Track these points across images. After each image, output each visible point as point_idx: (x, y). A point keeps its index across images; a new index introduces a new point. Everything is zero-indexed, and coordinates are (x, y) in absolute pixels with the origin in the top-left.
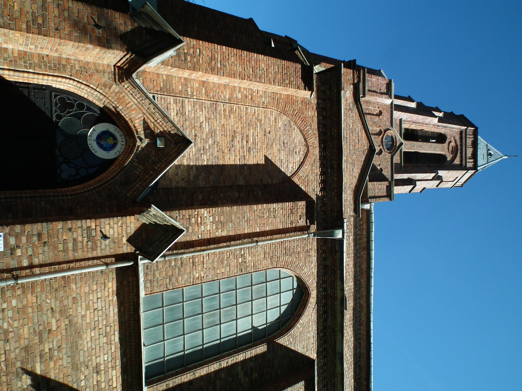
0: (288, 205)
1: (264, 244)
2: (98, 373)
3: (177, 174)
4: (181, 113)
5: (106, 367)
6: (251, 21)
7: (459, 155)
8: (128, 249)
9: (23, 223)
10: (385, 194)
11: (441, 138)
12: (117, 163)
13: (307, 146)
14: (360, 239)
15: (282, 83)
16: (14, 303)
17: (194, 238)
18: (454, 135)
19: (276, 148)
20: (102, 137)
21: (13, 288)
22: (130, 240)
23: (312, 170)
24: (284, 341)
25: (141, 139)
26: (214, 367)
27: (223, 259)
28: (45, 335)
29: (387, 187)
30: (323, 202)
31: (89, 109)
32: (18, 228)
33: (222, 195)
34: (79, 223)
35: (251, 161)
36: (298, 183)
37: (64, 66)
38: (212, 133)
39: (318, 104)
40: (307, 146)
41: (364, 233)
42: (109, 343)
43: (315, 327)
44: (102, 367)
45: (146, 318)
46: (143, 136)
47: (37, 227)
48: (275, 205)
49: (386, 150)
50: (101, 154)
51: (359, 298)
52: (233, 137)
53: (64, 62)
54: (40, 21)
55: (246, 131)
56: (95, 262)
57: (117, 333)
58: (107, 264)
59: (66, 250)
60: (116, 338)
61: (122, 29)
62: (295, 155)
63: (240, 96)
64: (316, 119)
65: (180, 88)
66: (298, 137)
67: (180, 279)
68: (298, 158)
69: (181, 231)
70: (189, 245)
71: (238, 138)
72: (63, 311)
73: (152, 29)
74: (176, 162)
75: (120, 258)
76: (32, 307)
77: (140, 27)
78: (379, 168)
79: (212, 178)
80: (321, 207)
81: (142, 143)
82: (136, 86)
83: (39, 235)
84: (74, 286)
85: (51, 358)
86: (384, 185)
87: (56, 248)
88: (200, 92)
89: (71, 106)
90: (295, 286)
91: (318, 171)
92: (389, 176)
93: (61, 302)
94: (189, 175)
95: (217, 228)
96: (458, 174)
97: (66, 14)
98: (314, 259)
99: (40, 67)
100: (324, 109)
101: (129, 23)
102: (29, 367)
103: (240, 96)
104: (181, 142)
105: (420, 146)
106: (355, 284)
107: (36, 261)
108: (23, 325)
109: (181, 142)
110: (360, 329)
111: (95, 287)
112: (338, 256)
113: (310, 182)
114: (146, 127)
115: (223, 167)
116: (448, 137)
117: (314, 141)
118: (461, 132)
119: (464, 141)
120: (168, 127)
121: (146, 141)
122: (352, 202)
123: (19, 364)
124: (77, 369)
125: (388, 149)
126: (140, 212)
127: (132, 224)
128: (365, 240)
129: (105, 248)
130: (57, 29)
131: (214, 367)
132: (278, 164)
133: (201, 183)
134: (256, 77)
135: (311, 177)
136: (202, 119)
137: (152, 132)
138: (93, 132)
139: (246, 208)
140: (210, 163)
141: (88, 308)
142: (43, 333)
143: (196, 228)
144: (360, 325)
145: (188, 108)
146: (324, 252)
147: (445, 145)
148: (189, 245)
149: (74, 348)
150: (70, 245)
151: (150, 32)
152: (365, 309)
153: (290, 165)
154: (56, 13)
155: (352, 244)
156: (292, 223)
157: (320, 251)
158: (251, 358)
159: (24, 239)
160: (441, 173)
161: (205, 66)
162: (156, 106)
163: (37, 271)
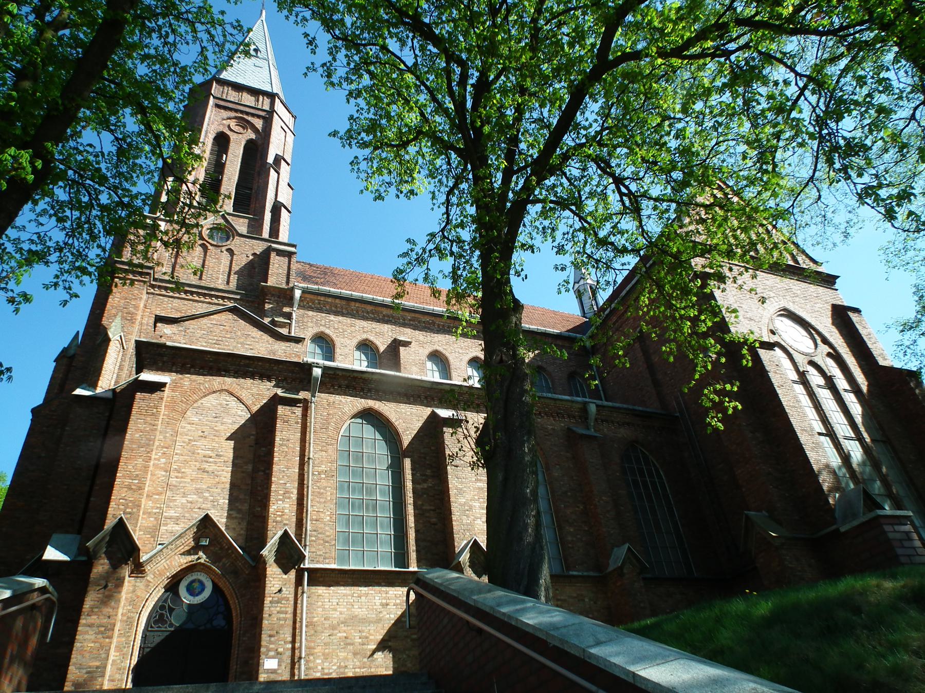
0: (279, 425)
1: (313, 451)
2: (387, 605)
3: (234, 529)
4: (177, 520)
5: (385, 598)
6: (34, 411)
7: (250, 118)
8: (292, 574)
9: (259, 646)
10: (286, 259)
11: (222, 141)
12: (216, 581)
13: (221, 391)
14: (336, 307)
15: (155, 416)
16: (319, 661)
17: (294, 519)
18: (219, 119)
19: (220, 427)
20: (191, 591)
21: (307, 662)
22: (286, 572)
23: (248, 389)
24: (406, 440)
25: (199, 558)
26: (410, 510)
27: (319, 493)
28: (349, 641)
29: (277, 255)
30: (282, 381)
31: (165, 601)
32: (263, 650)
33: (259, 488)
34: (266, 609)
35: (230, 455)
36: (259, 406)
37: (128, 618)
38: (198, 492)
39: (177, 372)
40: (221, 391)
41: (330, 300)
42: (367, 595)
43: (403, 406)
44: (384, 601)
45: (355, 565)
46: (196, 557)
47: (264, 637)
48: (277, 439)
49: (228, 242)
50: (207, 593)
51: (404, 320)
52: (204, 471)
53: (125, 618)
54: (103, 629)
55: (199, 457)
56: (299, 602)
57: (360, 588)
58: (303, 593)
59: (285, 619)
60: (364, 589)
61: (107, 567)
62: (227, 405)
63: (163, 460)
64: (194, 377)
65: (152, 519)
66: (211, 400)
67: (328, 533)
68: (233, 402)
69: (286, 532)
70: (300, 524)
71: (206, 466)
72: (333, 627)
73: (108, 542)
74: (223, 529)
75: (299, 582)
77: (105, 553)
78: (251, 257)
79: (242, 496)
80: (287, 383)
81: (203, 557)
82: (150, 560)
83: (271, 636)
84: (315, 619)
85: (367, 638)
86: (275, 259)
87: (282, 626)
88: (158, 500)
89: (161, 615)
90: (360, 421)
91: (249, 381)
92: (265, 245)
93: (325, 629)
94: (236, 518)
95: (289, 498)
96: (276, 123)
97: (96, 610)
98: (338, 398)
99: (129, 636)
100: (183, 365)
101: (102, 561)
102: (369, 653)
103: (163, 460)
104: (206, 523)
105: (230, 179)
106: (387, 322)
107: (290, 639)
108: (337, 656)
109: (206, 523)
110: (439, 325)
111: (320, 603)
112: (340, 373)
113: (259, 392)
114: (188, 553)
115: (233, 485)
116: (221, 129)
117: (217, 382)
118: (217, 106)
119: (231, 105)
120: (190, 535)
121: (201, 553)
122: (288, 344)
123: (365, 660)
124: (380, 620)
125: (228, 239)
126: (265, 563)
127: (273, 571)
128: (337, 301)
129: (289, 592)
130: (109, 617)
131: (410, 510)
132: (237, 426)
133: (245, 507)
134: (148, 445)
135: (255, 391)
136: (184, 500)
137: (193, 548)
138: (186, 599)
139: (275, 468)
140: (227, 497)
141: (335, 610)
142: (347, 642)
143: (285, 517)
144: (434, 323)
145: (172, 513)
146: (333, 386)
147: (233, 136)
148: (300, 524)
149: (364, 621)
150: (282, 616)
151: (109, 544)
152: (417, 315)
153: (240, 413)
154: (95, 617)
155: (341, 318)
156: (297, 423)
157: (332, 390)
158: (413, 474)
159: (272, 646)
160: (270, 159)
161: (136, 495)
162: (171, 543)
163: (297, 645)
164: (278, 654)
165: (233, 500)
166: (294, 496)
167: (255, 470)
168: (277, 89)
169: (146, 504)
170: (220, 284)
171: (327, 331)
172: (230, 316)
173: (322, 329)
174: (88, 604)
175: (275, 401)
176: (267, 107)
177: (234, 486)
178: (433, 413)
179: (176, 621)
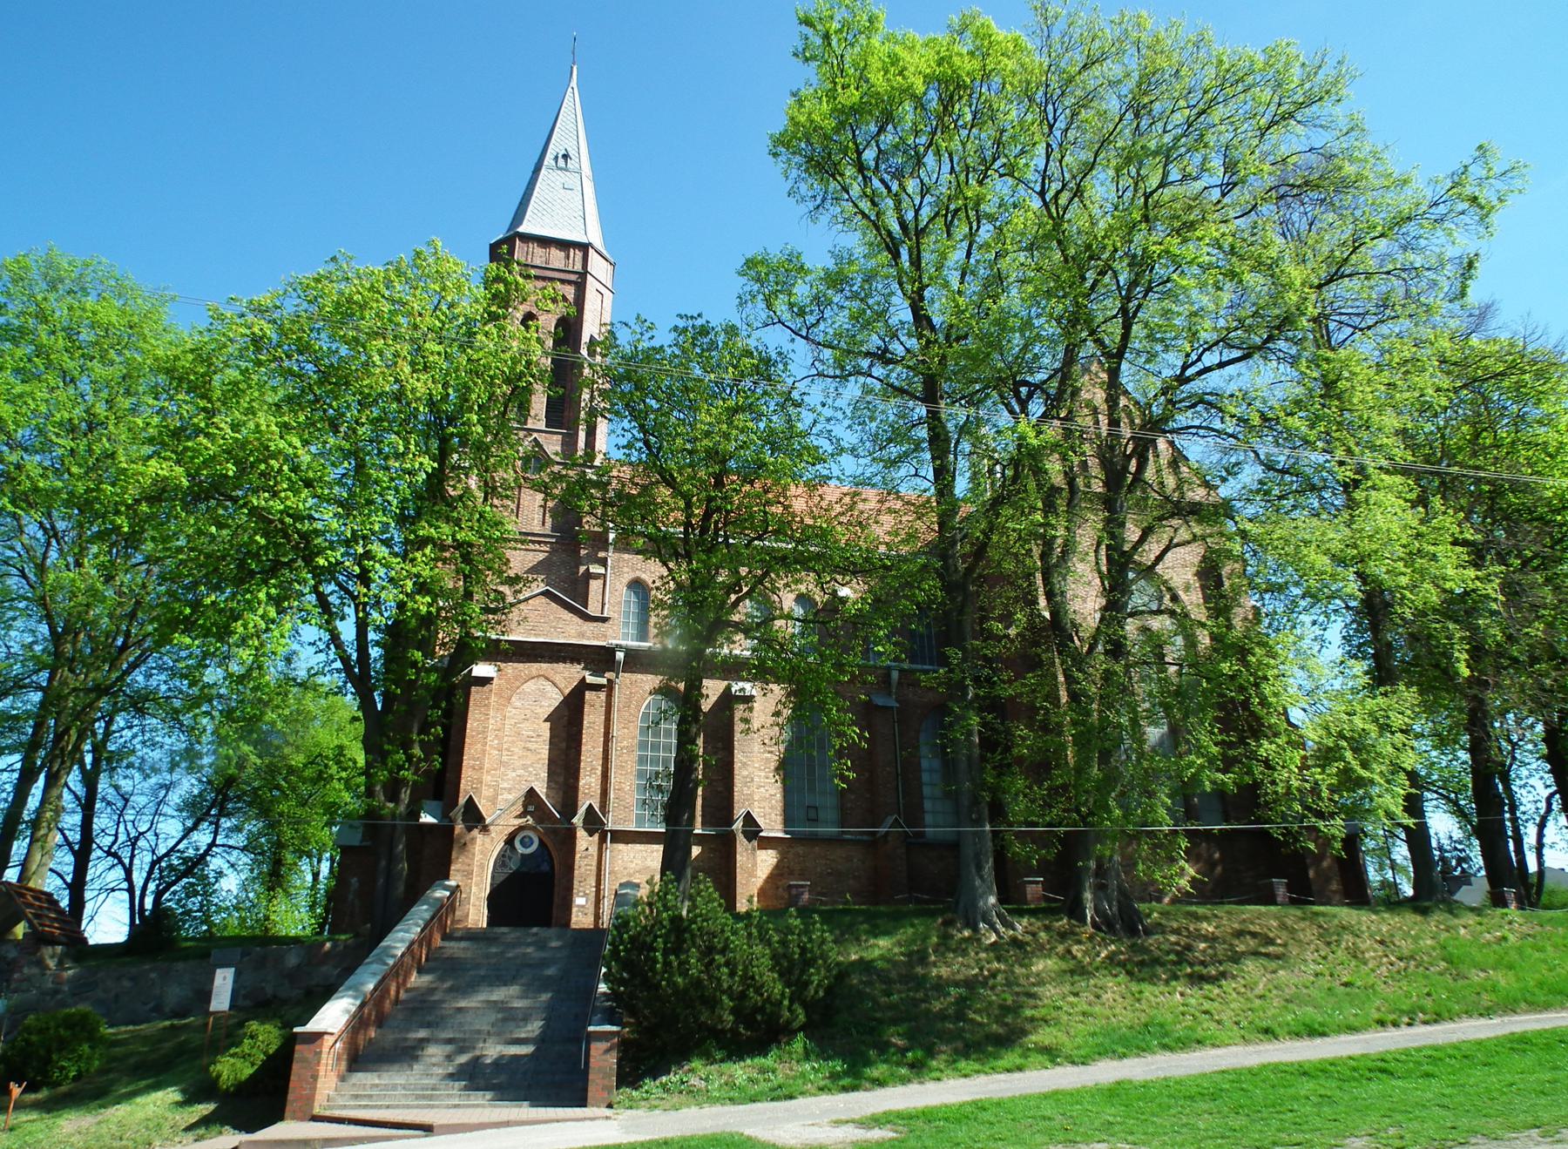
1: (616, 730)
4: (509, 790)
8: (596, 836)
19: (539, 710)
20: (522, 843)
38: (525, 767)
62: (543, 689)
68: (549, 687)
71: (529, 745)
75: (602, 840)
76: (1046, 525)
81: (530, 820)
91: (561, 665)
113: (569, 675)
117: (535, 668)
120: (520, 803)
127: (581, 834)
129: (594, 850)
133: (561, 779)
138: (520, 850)
164: (585, 895)
165: (551, 773)
166: (599, 772)
167: (568, 748)
168: (595, 237)
169: (487, 778)
170: (537, 529)
171: (643, 576)
172: (544, 600)
173: (638, 574)
174: (454, 855)
175: (583, 686)
176: (578, 267)
177: (551, 761)
178: (728, 688)
179: (513, 866)
